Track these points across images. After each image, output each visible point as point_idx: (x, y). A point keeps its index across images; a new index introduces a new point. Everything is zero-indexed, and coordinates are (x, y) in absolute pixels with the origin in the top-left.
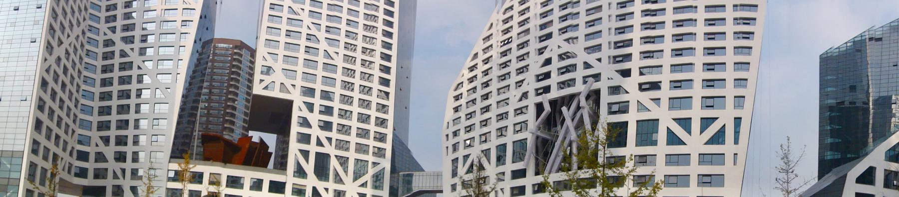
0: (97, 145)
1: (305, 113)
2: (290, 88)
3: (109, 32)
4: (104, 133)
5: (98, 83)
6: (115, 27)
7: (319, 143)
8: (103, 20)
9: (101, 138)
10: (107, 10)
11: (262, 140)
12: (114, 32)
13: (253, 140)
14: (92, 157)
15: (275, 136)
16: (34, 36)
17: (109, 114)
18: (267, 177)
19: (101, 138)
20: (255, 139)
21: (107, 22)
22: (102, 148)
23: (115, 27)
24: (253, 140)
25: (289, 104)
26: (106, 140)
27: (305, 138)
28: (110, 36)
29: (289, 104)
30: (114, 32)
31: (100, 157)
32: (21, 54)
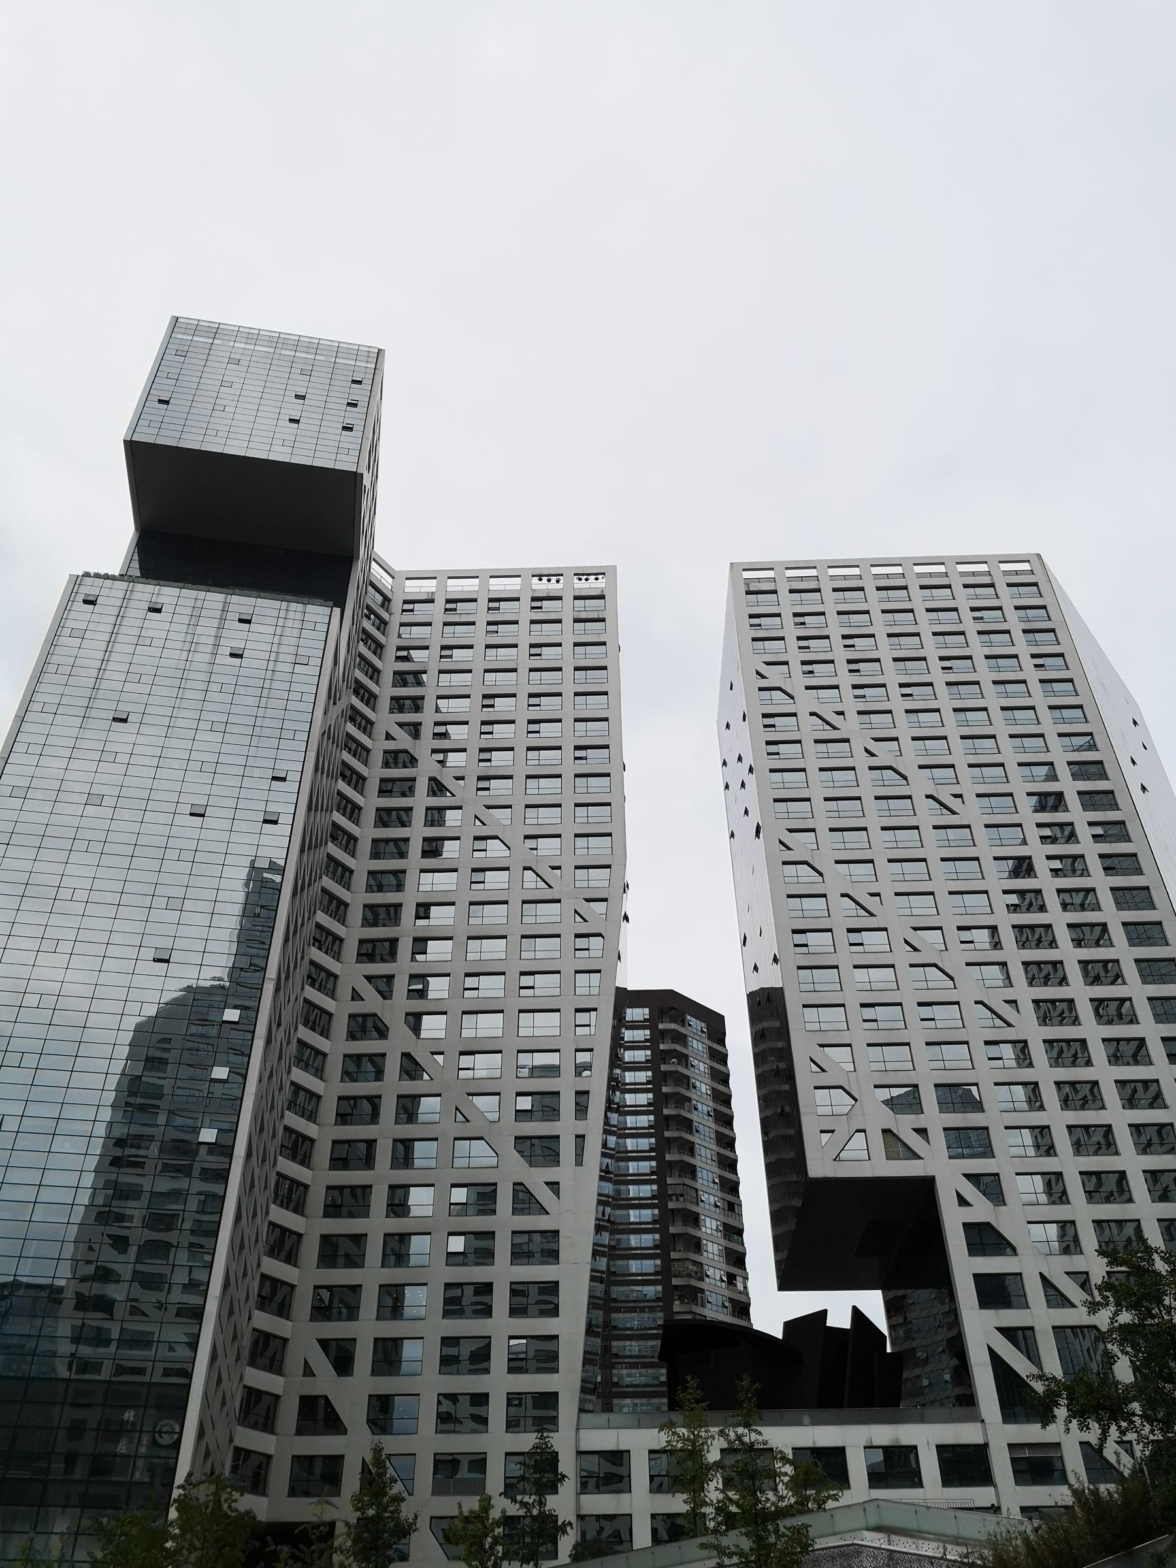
0: (308, 1371)
1: (981, 1210)
2: (914, 1141)
3: (367, 990)
4: (336, 1330)
5: (310, 1249)
6: (390, 978)
7: (1056, 1297)
8: (350, 949)
9: (324, 1344)
10: (343, 1118)
11: (857, 1313)
12: (386, 994)
13: (830, 1322)
14: (289, 1413)
15: (848, 1326)
16: (272, 808)
17: (352, 1314)
18: (925, 1437)
19: (324, 1344)
20: (840, 1319)
21: (321, 1312)
22: (326, 1382)
23: (390, 978)
24: (830, 1322)
25: (927, 1185)
26: (341, 1357)
27: (996, 1292)
28: (372, 1002)
29: (927, 1185)
30: (386, 994)
31: (319, 1415)
32: (50, 1047)
